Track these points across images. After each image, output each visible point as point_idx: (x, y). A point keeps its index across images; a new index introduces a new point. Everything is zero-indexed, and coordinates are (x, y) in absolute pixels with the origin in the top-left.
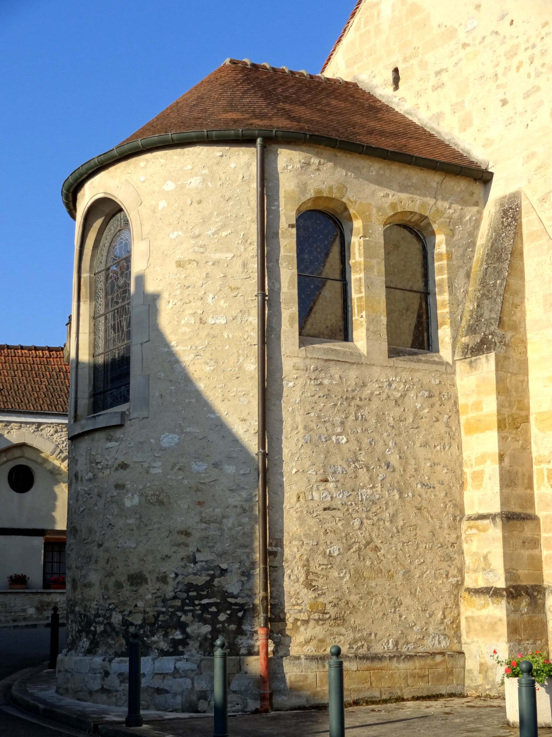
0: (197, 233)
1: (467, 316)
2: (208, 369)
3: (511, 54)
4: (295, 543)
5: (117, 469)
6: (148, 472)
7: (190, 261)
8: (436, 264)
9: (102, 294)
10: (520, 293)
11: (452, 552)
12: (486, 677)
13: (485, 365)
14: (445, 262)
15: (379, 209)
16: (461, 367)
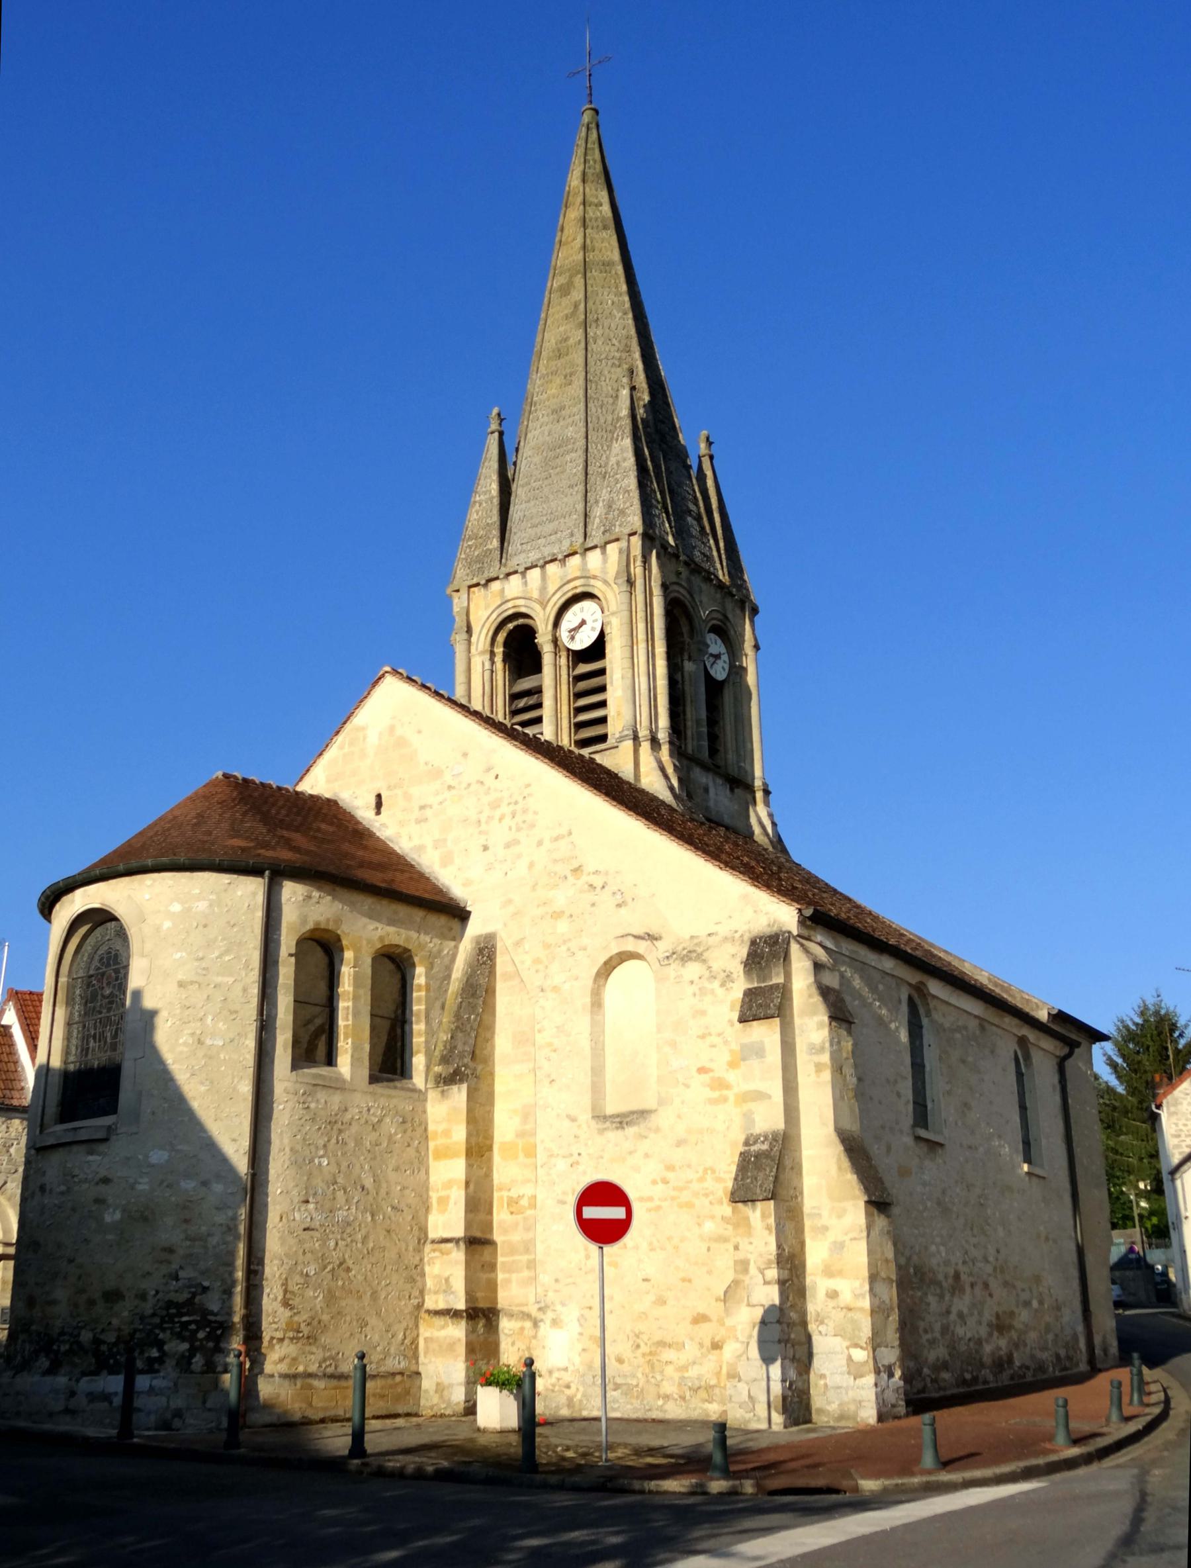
0: (201, 955)
1: (440, 1046)
2: (203, 1088)
3: (495, 805)
4: (276, 1262)
5: (97, 1184)
7: (192, 983)
8: (415, 994)
9: (78, 999)
10: (491, 1028)
11: (415, 1275)
12: (441, 1397)
13: (457, 1096)
14: (423, 993)
16: (432, 1095)
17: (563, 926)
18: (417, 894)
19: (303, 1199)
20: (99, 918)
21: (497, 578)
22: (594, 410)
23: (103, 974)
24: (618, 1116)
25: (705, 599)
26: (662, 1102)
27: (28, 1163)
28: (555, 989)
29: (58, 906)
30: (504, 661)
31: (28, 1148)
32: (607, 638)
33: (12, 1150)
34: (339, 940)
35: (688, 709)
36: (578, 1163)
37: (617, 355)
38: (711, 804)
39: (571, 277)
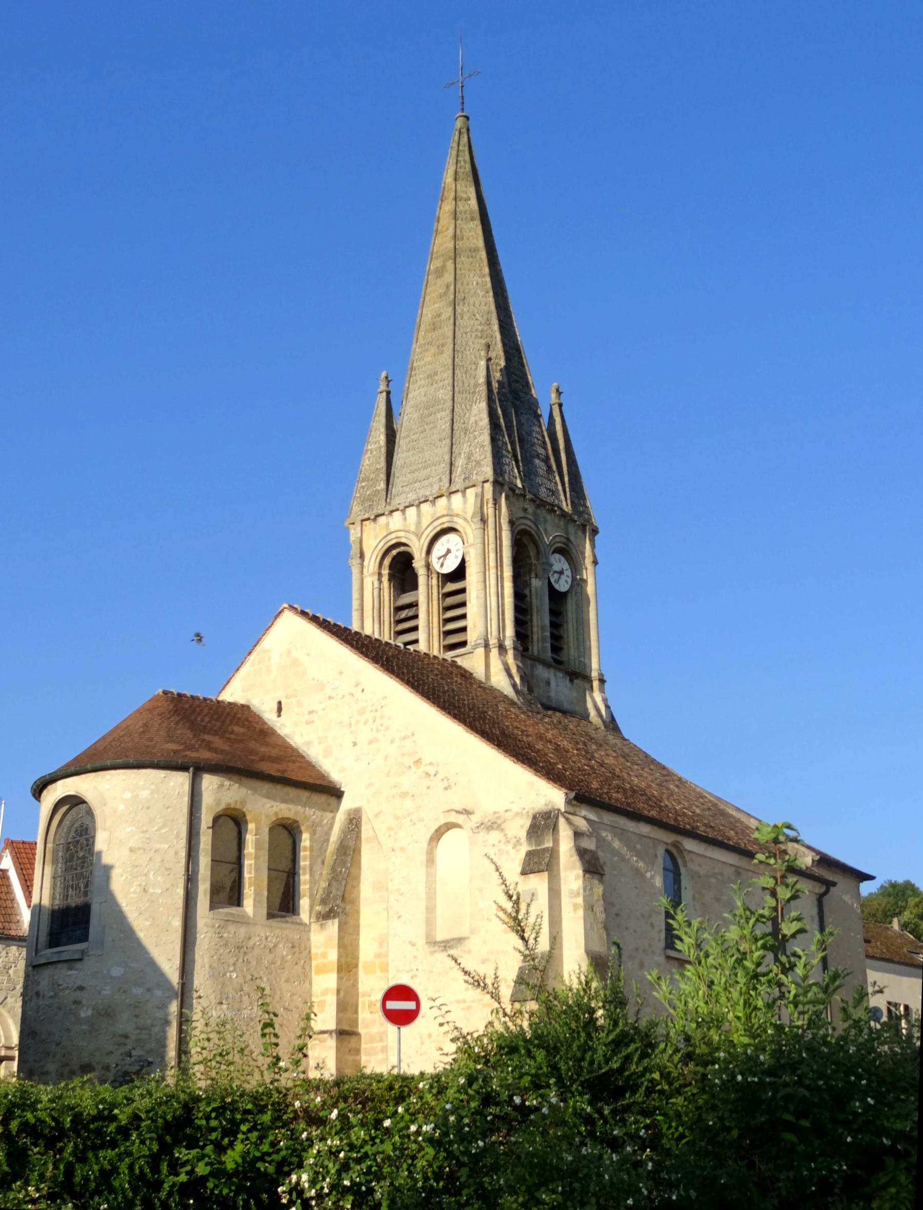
0: (145, 829)
1: (321, 892)
2: (147, 923)
3: (361, 712)
5: (75, 990)
6: (100, 993)
7: (139, 849)
9: (60, 860)
10: (357, 878)
14: (308, 853)
15: (267, 816)
17: (408, 803)
18: (303, 780)
19: (218, 1001)
20: (73, 802)
21: (383, 514)
22: (460, 376)
23: (78, 842)
24: (443, 942)
25: (549, 528)
26: (472, 932)
27: (27, 976)
28: (402, 849)
29: (45, 792)
30: (390, 580)
31: (27, 966)
32: (467, 564)
33: (11, 972)
34: (244, 815)
35: (535, 618)
36: (416, 976)
37: (480, 328)
38: (552, 694)
39: (444, 262)
